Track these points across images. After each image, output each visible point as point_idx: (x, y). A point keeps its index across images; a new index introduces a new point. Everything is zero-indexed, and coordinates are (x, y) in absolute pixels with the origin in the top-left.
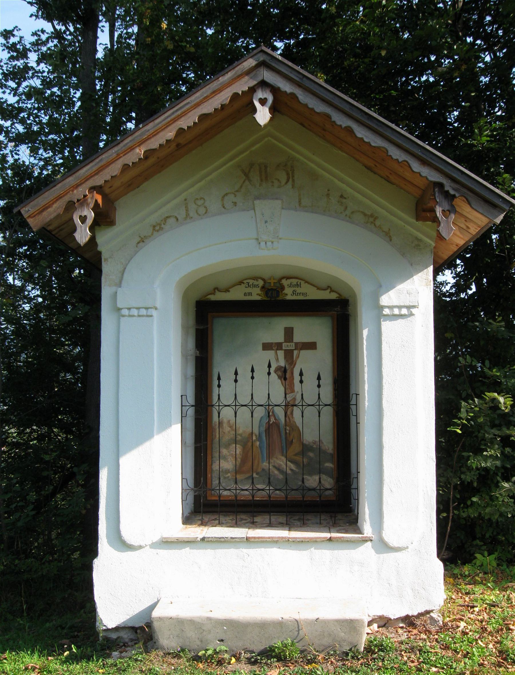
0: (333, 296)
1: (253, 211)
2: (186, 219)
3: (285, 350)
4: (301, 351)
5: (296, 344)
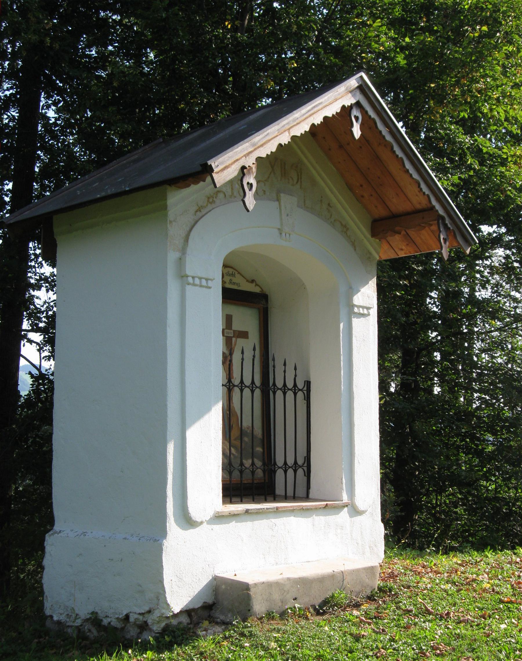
0: (257, 290)
1: (277, 203)
2: (231, 197)
3: (226, 337)
4: (238, 339)
5: (234, 331)
